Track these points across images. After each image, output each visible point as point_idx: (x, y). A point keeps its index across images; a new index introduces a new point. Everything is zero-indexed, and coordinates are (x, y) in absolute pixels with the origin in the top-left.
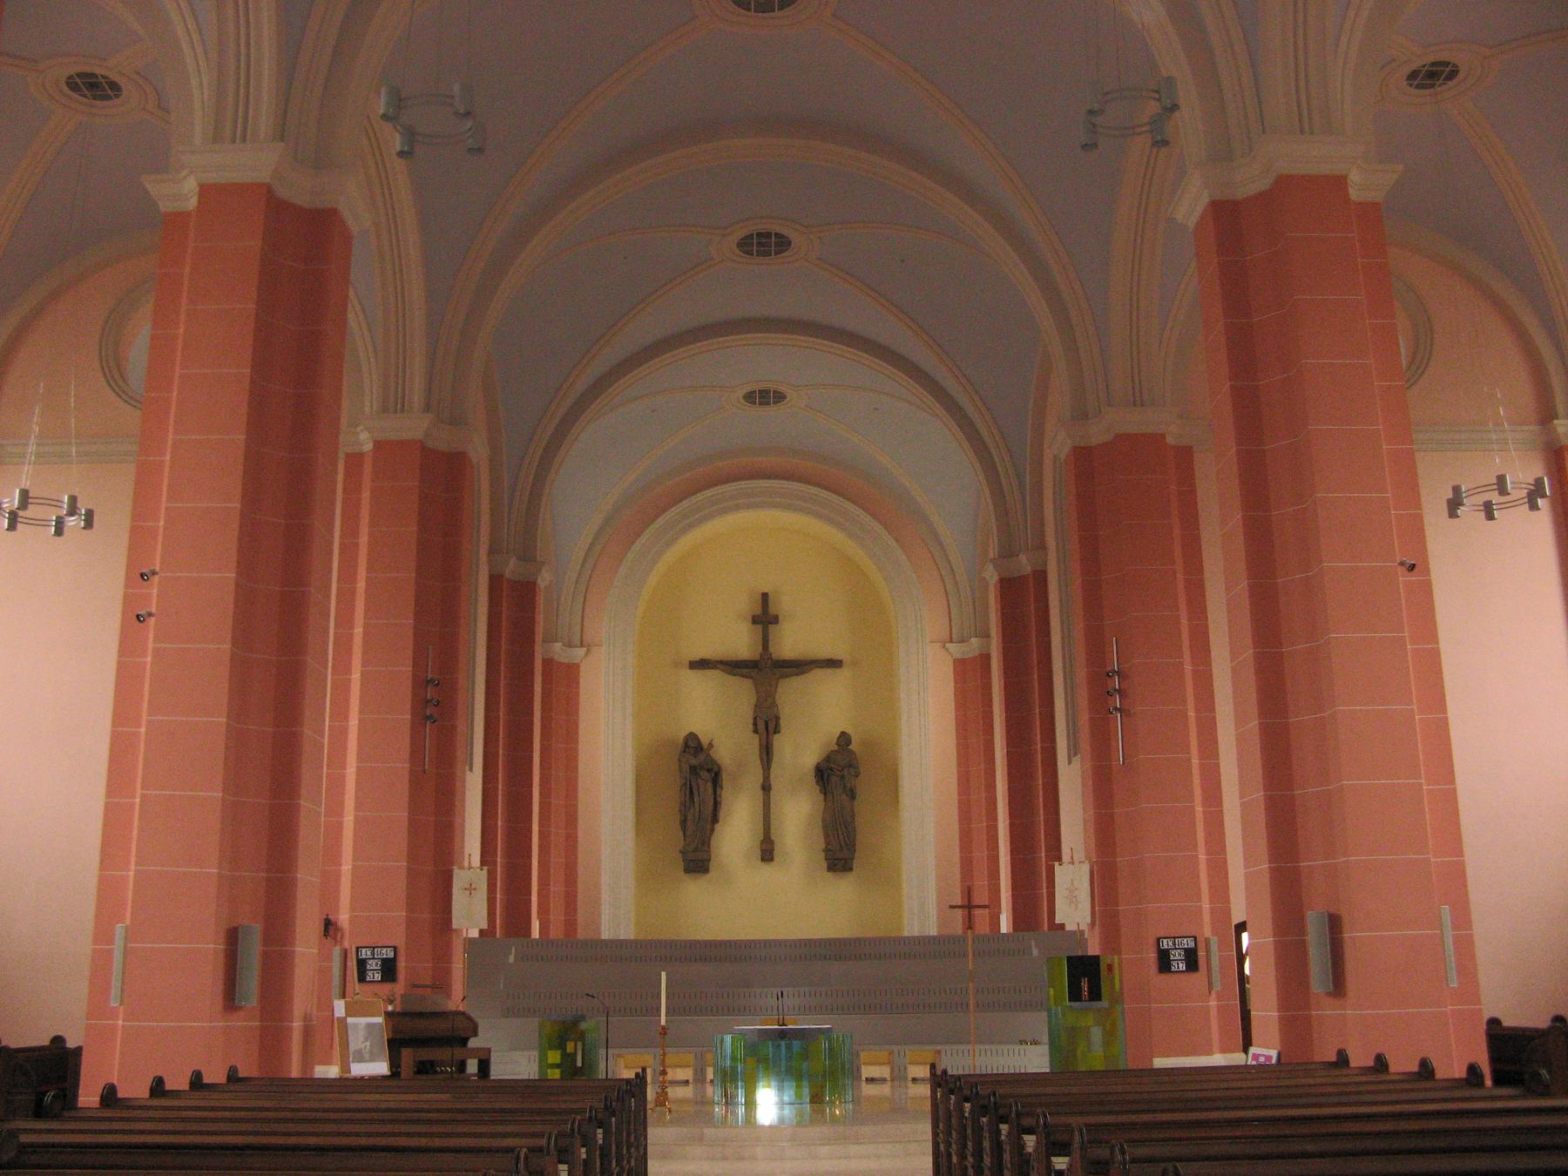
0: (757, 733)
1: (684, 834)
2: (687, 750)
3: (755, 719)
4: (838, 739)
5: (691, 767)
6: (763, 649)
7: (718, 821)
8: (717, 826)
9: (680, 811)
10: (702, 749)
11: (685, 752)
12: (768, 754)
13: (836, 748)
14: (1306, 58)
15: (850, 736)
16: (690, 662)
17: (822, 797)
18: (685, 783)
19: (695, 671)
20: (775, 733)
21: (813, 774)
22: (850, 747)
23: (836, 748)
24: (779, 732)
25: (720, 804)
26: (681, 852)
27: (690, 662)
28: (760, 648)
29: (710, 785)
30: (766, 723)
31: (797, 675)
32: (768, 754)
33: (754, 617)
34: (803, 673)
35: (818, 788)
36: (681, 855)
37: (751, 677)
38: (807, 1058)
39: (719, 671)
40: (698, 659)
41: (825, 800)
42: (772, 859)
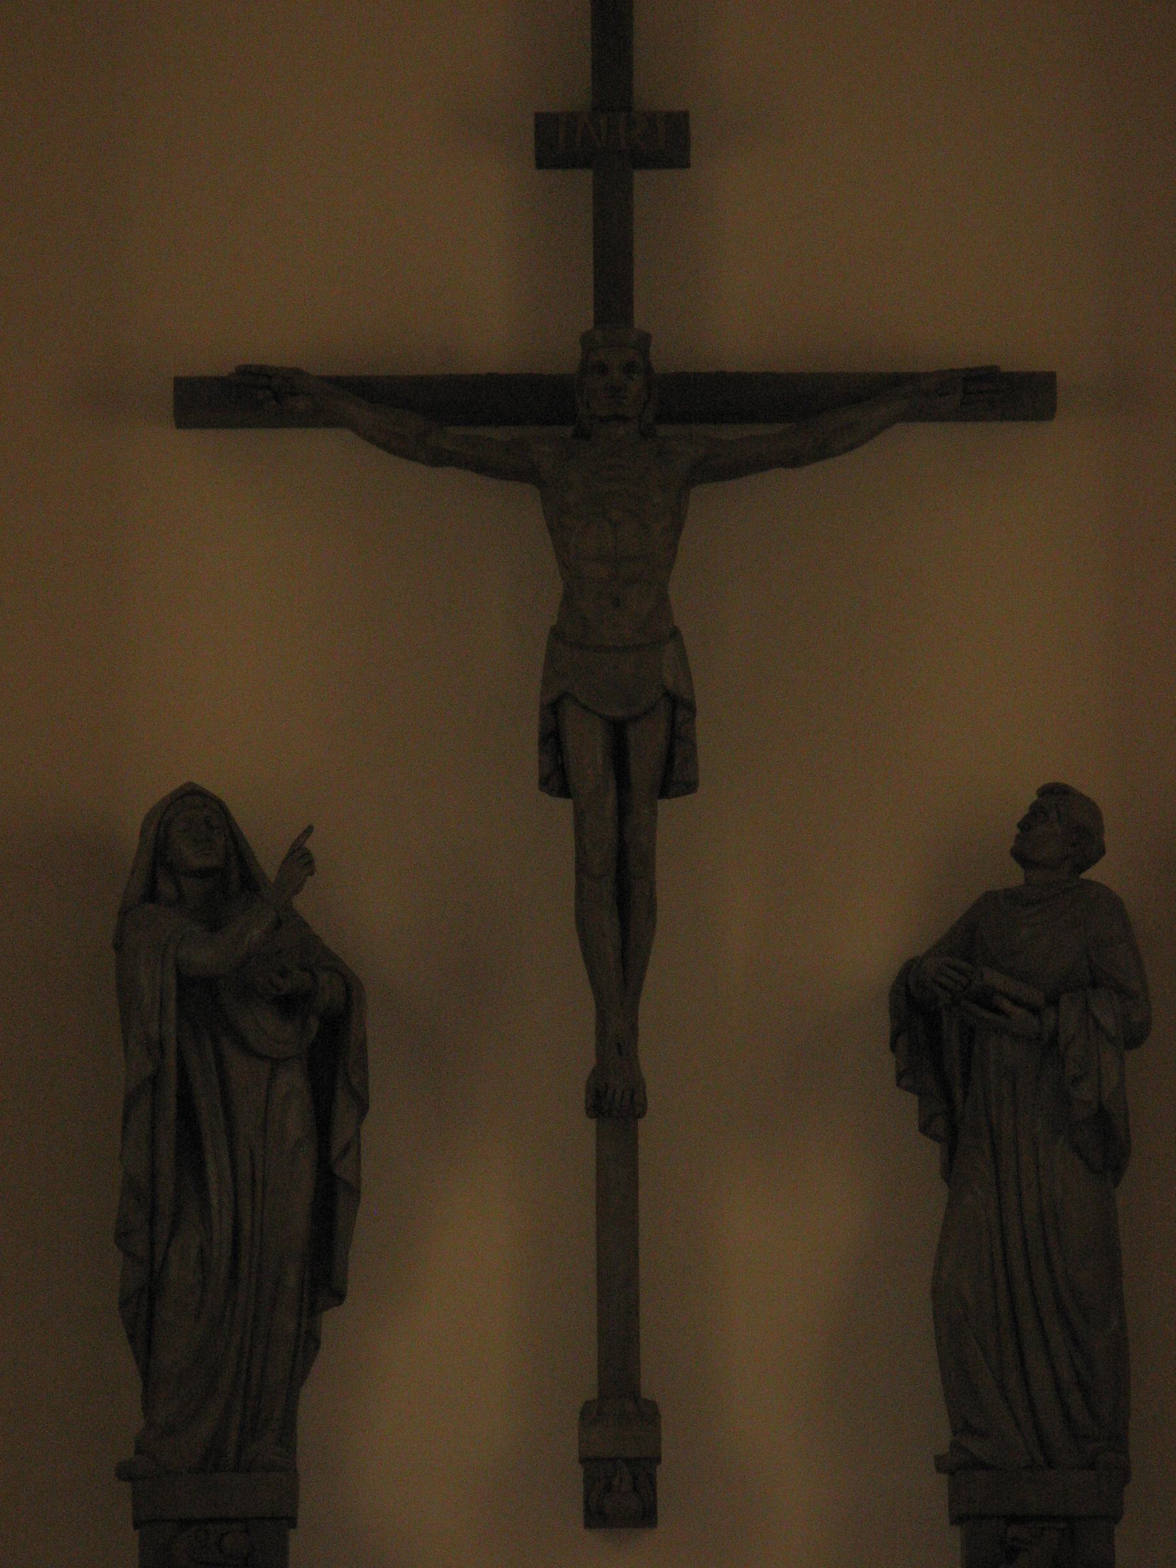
0: (564, 791)
1: (146, 1374)
2: (166, 888)
3: (553, 709)
4: (1025, 826)
5: (186, 983)
6: (599, 320)
7: (339, 1296)
8: (331, 1321)
9: (123, 1235)
10: (250, 881)
11: (151, 894)
12: (623, 899)
13: (1014, 875)
14: (236, 1211)
15: (1095, 813)
16: (178, 381)
17: (931, 1152)
18: (154, 1082)
19: (194, 433)
20: (664, 791)
21: (881, 1023)
22: (1090, 874)
23: (1014, 875)
24: (690, 787)
25: (355, 1192)
26: (124, 1472)
27: (178, 381)
28: (585, 318)
29: (293, 1080)
30: (618, 732)
31: (794, 460)
32: (623, 899)
33: (545, 124)
34: (823, 452)
35: (909, 1103)
36: (126, 1487)
37: (527, 474)
38: (618, 606)
39: (347, 434)
40: (226, 369)
41: (949, 1170)
42: (647, 1516)
